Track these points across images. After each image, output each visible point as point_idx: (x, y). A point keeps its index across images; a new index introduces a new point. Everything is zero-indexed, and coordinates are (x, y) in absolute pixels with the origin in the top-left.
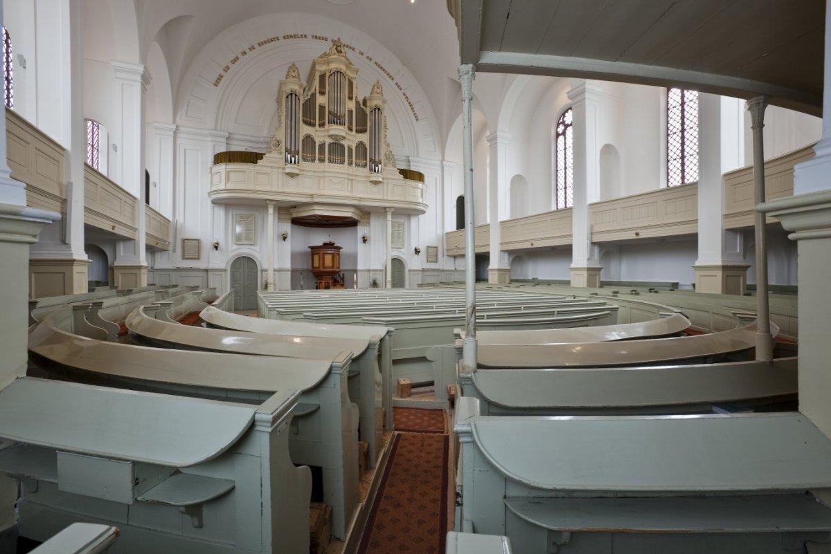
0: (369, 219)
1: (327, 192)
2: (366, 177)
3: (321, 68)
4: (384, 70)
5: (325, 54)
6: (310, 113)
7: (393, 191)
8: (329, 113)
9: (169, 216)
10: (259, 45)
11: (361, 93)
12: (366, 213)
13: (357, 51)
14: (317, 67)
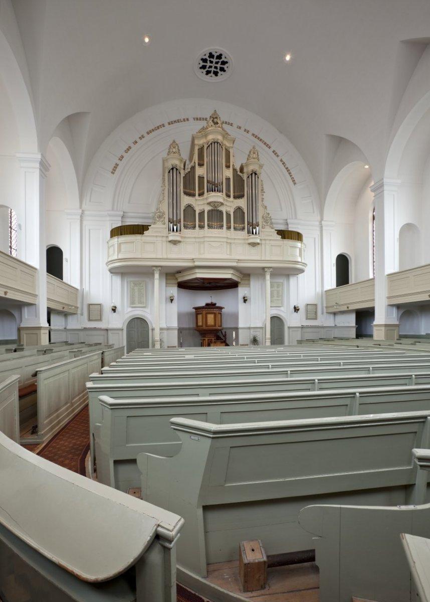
0: (250, 278)
2: (244, 239)
3: (200, 142)
4: (261, 140)
5: (203, 129)
6: (191, 185)
8: (208, 182)
9: (77, 286)
11: (236, 162)
12: (247, 274)
13: (235, 126)
14: (196, 142)
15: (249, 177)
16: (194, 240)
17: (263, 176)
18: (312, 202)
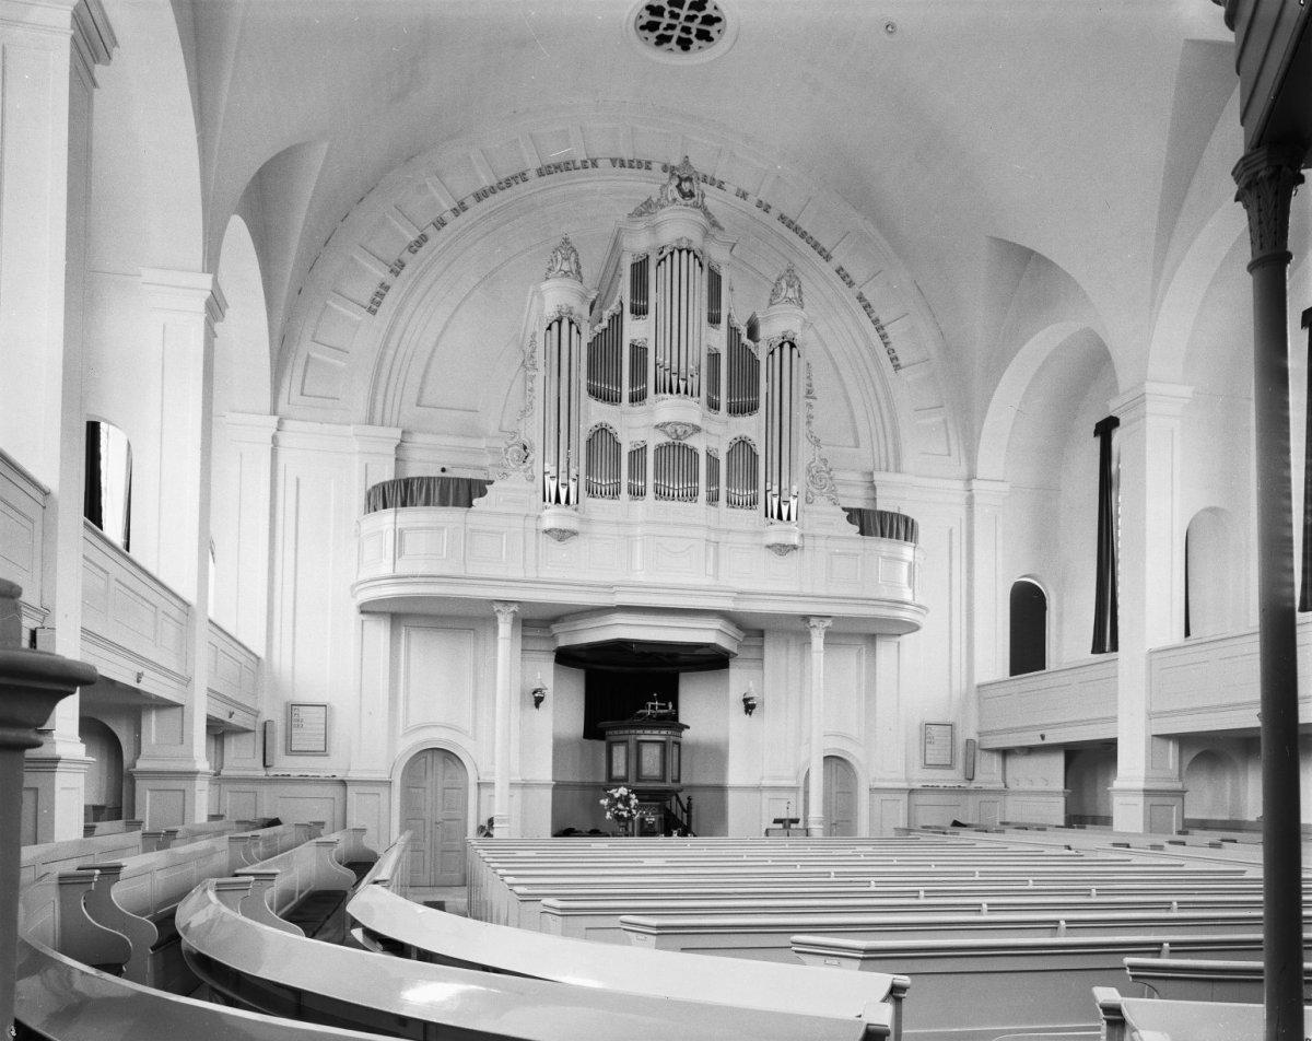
3: (639, 242)
11: (737, 308)
12: (754, 631)
14: (626, 243)
15: (772, 353)
18: (945, 422)
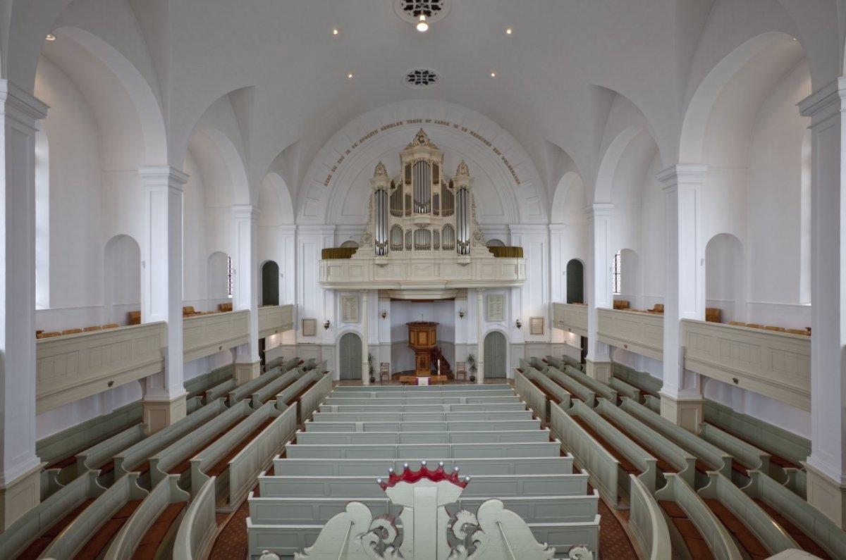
1: (413, 279)
2: (454, 259)
3: (408, 159)
7: (483, 269)
8: (415, 201)
10: (361, 141)
12: (462, 292)
16: (400, 262)
17: (473, 191)
18: (539, 202)
